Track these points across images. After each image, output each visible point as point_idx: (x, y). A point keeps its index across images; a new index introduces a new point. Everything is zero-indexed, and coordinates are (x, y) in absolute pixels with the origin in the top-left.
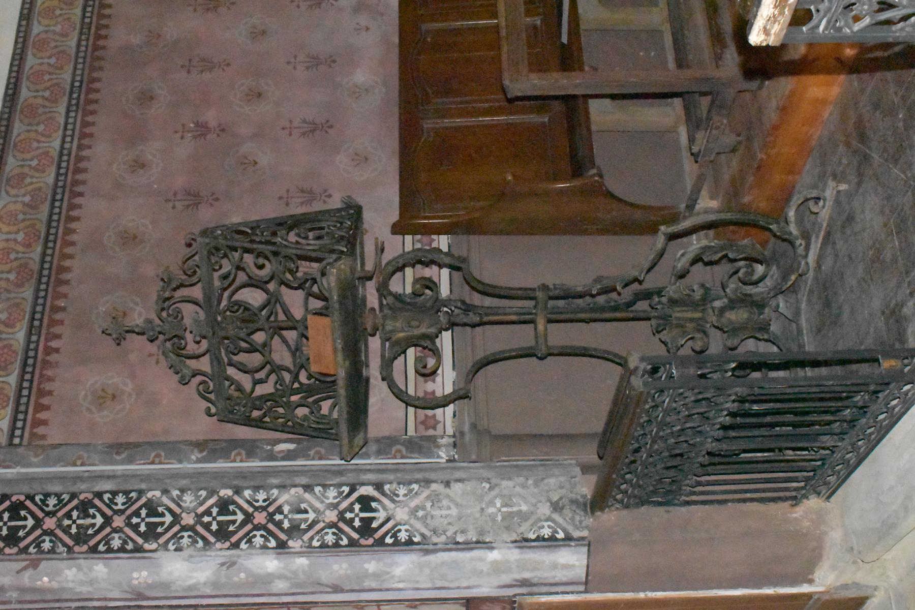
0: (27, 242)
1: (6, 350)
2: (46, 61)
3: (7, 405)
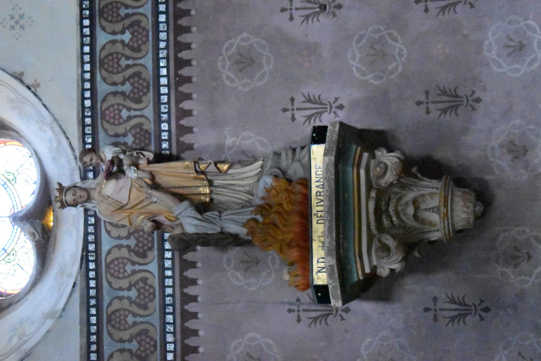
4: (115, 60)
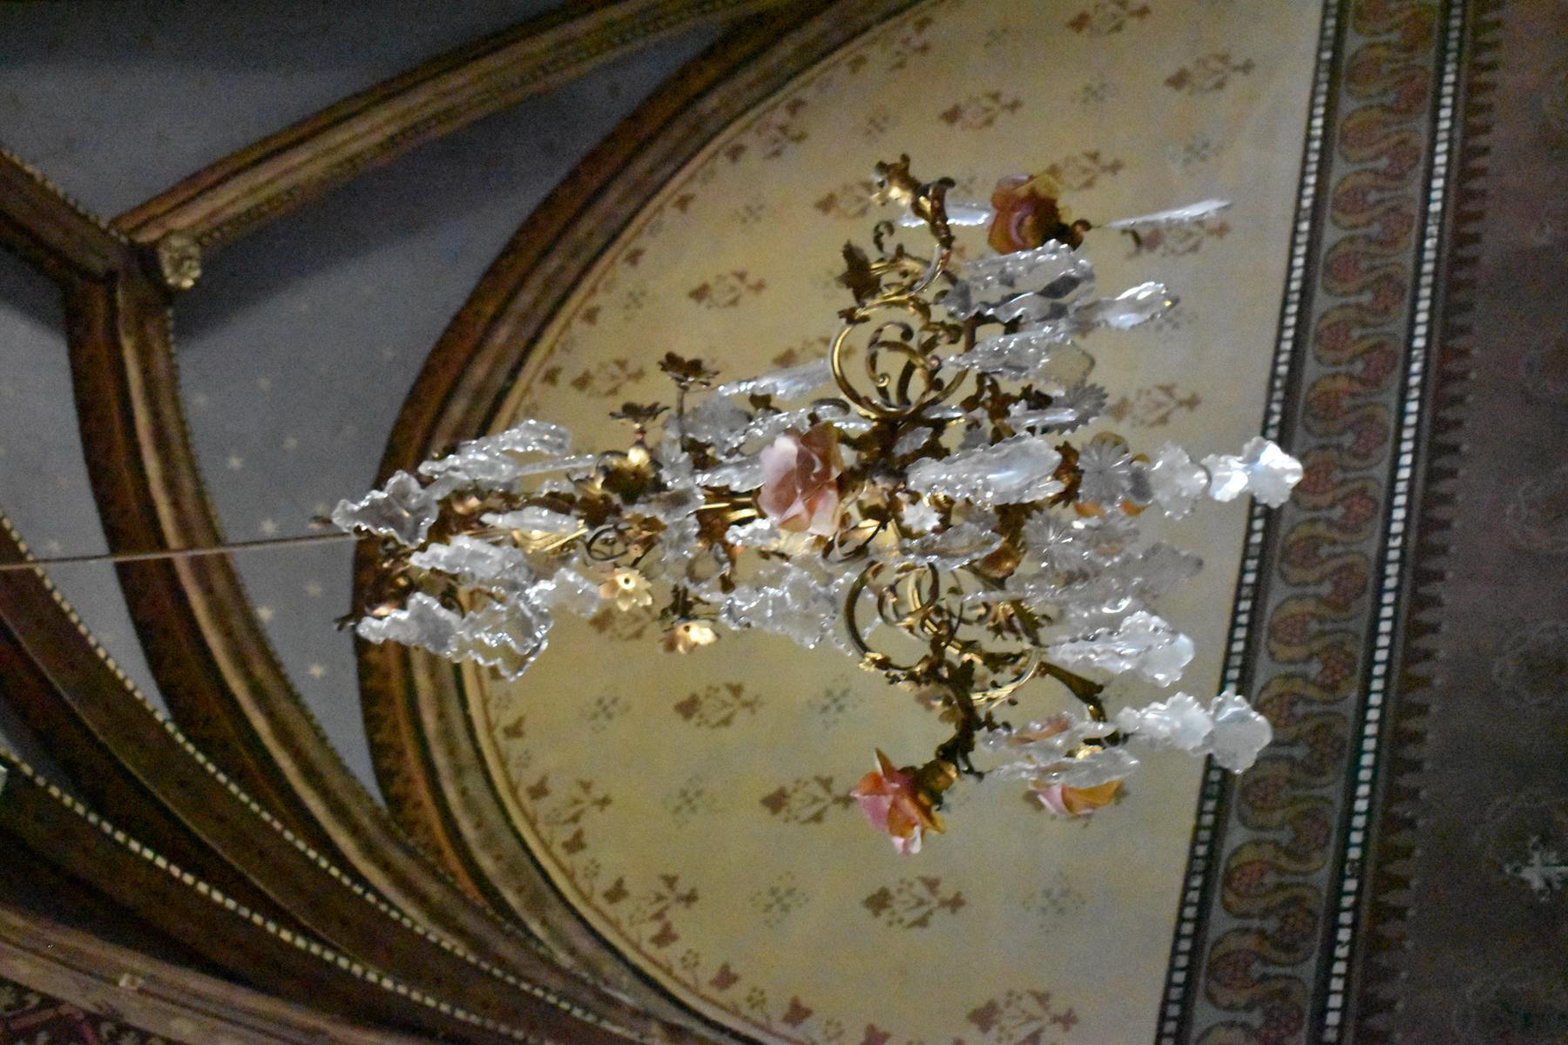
0: (1287, 940)
1: (1292, 910)
2: (1352, 300)
3: (1300, 1027)
4: (1322, 474)
